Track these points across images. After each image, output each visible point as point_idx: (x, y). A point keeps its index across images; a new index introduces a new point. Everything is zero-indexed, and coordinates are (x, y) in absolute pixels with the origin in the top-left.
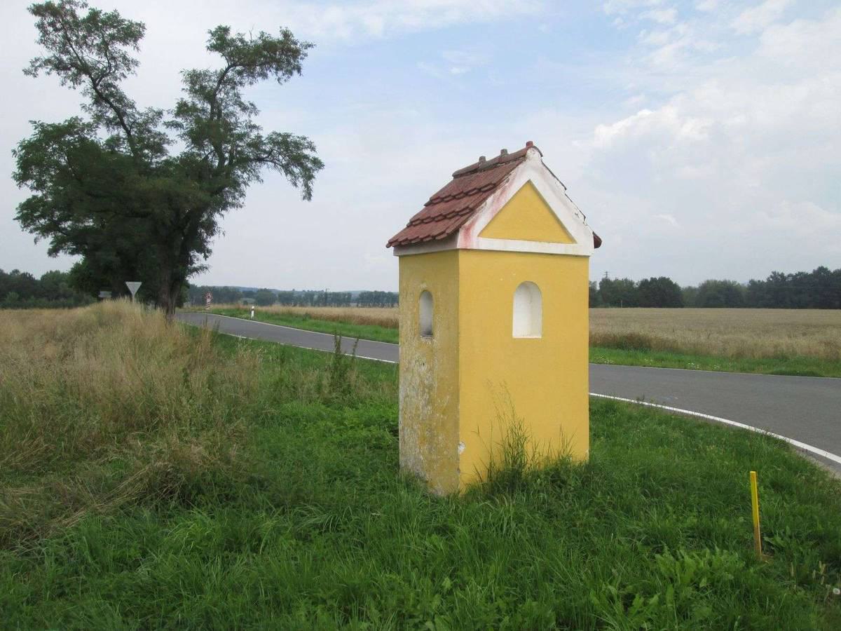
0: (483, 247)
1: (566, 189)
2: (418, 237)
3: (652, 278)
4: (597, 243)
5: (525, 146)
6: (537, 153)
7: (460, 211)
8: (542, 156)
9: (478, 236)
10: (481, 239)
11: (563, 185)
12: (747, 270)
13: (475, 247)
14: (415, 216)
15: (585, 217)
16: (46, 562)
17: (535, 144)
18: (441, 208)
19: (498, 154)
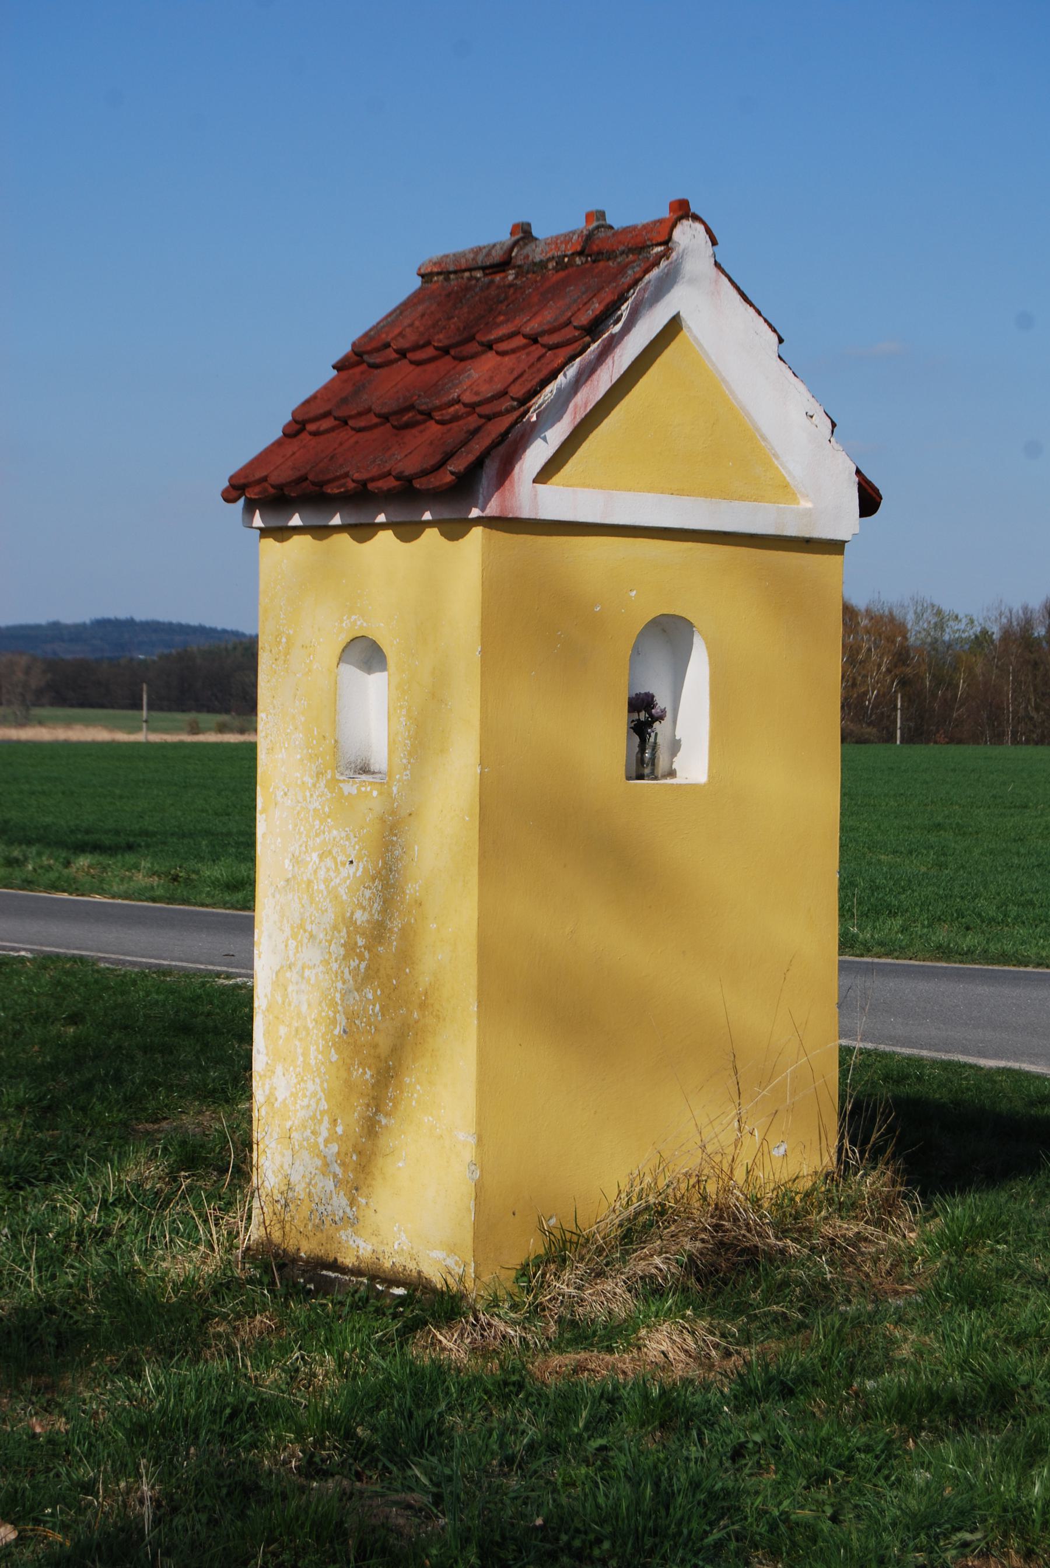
0: (548, 513)
1: (781, 340)
2: (265, 479)
3: (680, 740)
4: (869, 501)
5: (665, 213)
6: (700, 227)
7: (480, 404)
8: (714, 242)
9: (534, 481)
10: (540, 487)
11: (775, 331)
12: (751, 310)
13: (526, 513)
14: (307, 403)
15: (834, 425)
16: (869, 730)
17: (694, 209)
18: (390, 386)
19: (578, 223)
